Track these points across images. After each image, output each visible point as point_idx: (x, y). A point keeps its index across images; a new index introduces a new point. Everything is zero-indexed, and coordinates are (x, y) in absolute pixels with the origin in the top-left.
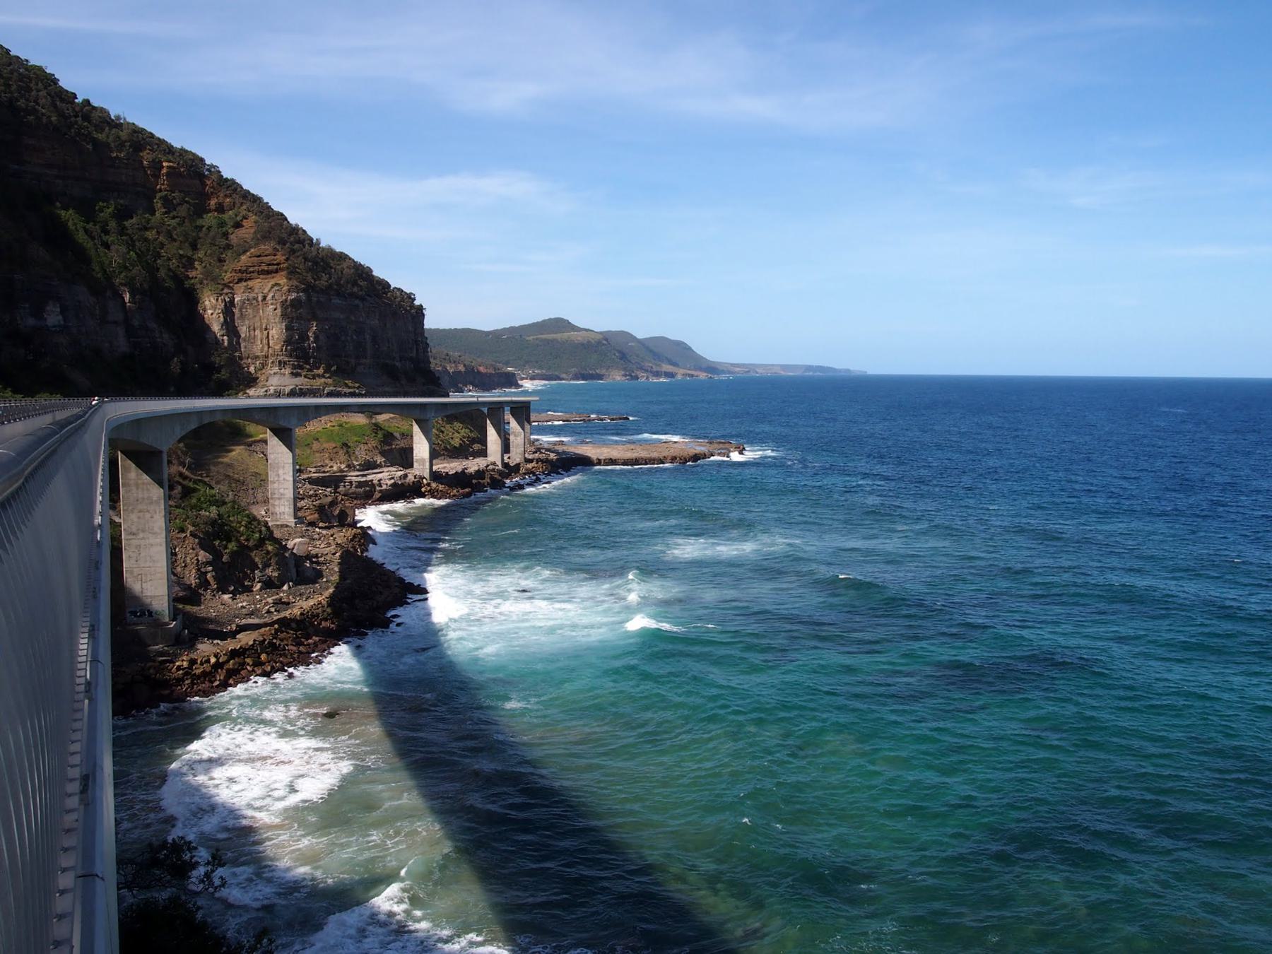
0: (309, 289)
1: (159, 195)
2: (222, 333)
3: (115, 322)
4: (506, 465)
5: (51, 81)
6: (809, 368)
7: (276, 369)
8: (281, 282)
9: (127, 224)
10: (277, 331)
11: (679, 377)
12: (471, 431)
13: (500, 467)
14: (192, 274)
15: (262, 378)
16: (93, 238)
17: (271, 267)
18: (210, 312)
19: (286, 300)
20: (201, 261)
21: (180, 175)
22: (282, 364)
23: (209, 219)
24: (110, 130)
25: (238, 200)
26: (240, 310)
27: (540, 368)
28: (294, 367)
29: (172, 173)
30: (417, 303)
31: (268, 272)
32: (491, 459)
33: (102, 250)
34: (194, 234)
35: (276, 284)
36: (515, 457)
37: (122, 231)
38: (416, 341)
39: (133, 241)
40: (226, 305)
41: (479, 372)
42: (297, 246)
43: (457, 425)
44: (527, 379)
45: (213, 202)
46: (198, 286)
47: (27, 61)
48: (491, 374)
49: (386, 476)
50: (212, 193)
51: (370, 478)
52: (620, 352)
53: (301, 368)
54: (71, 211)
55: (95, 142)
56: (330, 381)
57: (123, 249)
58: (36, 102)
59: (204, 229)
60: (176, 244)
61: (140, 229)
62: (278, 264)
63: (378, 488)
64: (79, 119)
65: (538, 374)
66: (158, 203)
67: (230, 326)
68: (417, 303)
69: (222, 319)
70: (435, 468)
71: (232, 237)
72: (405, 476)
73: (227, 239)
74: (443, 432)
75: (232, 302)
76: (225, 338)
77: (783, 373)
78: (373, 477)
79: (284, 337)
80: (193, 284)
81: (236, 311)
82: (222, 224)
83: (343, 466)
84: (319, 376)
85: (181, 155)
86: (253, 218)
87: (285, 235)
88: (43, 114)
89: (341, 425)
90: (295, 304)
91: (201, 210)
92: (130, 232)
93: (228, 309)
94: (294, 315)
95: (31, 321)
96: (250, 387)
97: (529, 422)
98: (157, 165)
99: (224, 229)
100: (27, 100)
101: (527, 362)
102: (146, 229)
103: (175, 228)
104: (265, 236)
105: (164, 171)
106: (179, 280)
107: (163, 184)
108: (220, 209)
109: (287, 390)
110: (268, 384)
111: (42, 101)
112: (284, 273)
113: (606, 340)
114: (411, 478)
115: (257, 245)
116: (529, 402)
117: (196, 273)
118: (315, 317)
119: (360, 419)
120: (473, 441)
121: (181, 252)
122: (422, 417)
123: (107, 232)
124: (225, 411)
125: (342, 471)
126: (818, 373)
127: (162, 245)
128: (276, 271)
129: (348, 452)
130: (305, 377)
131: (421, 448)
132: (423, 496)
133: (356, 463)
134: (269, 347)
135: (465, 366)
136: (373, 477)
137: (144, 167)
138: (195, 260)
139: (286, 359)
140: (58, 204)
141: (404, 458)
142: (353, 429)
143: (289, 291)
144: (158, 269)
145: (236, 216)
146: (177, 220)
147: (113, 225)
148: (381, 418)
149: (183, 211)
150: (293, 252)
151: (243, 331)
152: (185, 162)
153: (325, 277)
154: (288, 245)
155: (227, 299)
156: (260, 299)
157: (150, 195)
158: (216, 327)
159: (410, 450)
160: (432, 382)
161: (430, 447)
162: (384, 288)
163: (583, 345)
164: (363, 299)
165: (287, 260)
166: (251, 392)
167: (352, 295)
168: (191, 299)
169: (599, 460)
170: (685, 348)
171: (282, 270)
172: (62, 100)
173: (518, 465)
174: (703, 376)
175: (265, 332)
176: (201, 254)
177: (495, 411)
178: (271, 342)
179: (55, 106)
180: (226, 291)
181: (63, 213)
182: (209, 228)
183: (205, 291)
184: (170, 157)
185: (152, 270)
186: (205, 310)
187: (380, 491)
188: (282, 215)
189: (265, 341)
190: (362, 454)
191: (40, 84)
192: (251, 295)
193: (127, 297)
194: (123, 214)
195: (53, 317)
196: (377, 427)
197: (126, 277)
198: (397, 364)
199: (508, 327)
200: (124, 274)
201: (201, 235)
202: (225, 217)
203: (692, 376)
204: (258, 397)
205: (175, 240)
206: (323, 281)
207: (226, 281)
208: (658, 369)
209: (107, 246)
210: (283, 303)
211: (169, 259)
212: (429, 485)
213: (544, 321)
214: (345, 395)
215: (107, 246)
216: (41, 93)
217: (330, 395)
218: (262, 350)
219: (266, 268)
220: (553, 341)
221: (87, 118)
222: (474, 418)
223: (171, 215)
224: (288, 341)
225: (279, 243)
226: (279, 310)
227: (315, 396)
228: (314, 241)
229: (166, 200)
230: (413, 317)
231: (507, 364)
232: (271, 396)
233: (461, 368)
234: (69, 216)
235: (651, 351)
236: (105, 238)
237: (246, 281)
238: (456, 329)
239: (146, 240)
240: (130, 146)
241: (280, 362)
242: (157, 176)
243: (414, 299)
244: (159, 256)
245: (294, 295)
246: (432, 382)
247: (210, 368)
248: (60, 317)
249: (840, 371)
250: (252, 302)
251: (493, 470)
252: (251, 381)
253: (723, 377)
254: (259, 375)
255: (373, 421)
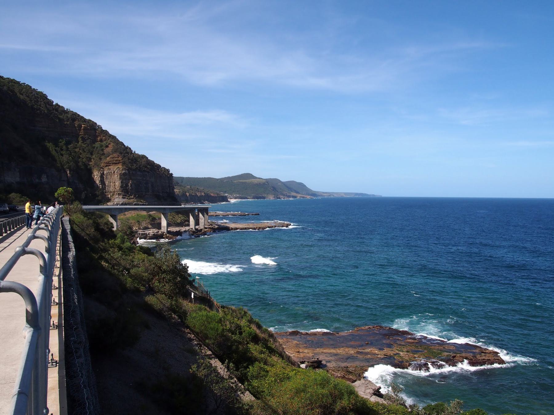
0: (129, 169)
1: (80, 136)
2: (100, 183)
3: (64, 181)
4: (196, 229)
5: (44, 97)
6: (357, 194)
7: (117, 196)
8: (120, 167)
9: (69, 146)
10: (118, 184)
11: (298, 198)
12: (185, 217)
13: (194, 230)
14: (91, 163)
15: (113, 199)
16: (57, 152)
17: (117, 162)
18: (96, 177)
19: (121, 173)
20: (94, 159)
21: (88, 129)
22: (119, 194)
23: (97, 145)
24: (65, 114)
25: (107, 137)
26: (106, 176)
27: (239, 194)
28: (123, 195)
29: (85, 129)
30: (170, 172)
31: (116, 163)
32: (191, 227)
33: (60, 156)
34: (92, 150)
35: (118, 168)
36: (201, 226)
37: (67, 149)
38: (169, 186)
39: (71, 153)
40: (101, 174)
41: (211, 196)
42: (126, 154)
43: (180, 215)
44: (233, 198)
45: (99, 138)
46: (92, 168)
47: (37, 90)
48: (216, 197)
49: (152, 232)
50: (99, 135)
51: (146, 232)
52: (273, 187)
53: (126, 196)
54: (51, 143)
55: (59, 119)
56: (135, 200)
57: (67, 156)
58: (40, 106)
59: (95, 148)
60: (86, 153)
61: (74, 148)
62: (119, 161)
63: (148, 236)
64: (54, 111)
65: (238, 197)
66: (80, 139)
67: (102, 181)
68: (170, 172)
69: (100, 179)
70: (168, 230)
71: (105, 151)
72: (158, 232)
73: (103, 151)
74: (174, 218)
75: (103, 174)
76: (101, 185)
77: (345, 196)
78: (147, 232)
79: (120, 185)
80: (91, 167)
81: (105, 176)
82: (102, 146)
83: (137, 228)
84: (132, 198)
85: (88, 122)
86: (112, 144)
87: (122, 151)
88: (42, 110)
89: (138, 215)
90: (124, 174)
91: (95, 141)
92: (70, 149)
93: (102, 176)
94: (124, 178)
95: (37, 180)
96: (108, 202)
97: (207, 214)
98: (80, 126)
99: (102, 148)
100: (37, 105)
101: (233, 192)
102: (76, 148)
103: (85, 148)
104: (115, 151)
105: (82, 128)
106: (86, 165)
107: (82, 132)
108: (101, 141)
109: (121, 203)
110: (114, 201)
111: (42, 106)
112: (121, 164)
113: (267, 182)
114: (160, 232)
115: (112, 154)
116: (208, 208)
117: (92, 163)
118: (131, 179)
119: (144, 213)
120: (186, 221)
121: (87, 156)
122: (164, 212)
123: (62, 150)
124: (94, 209)
125: (136, 230)
126: (360, 196)
127: (81, 154)
128: (119, 163)
129: (139, 224)
130: (127, 199)
131: (164, 223)
132: (163, 238)
133: (141, 227)
134: (115, 189)
135: (204, 193)
136: (147, 232)
137: (75, 127)
138: (92, 159)
139: (121, 193)
140: (47, 141)
141: (159, 226)
142: (142, 216)
143: (122, 170)
144: (79, 162)
145: (107, 143)
146: (86, 145)
147: (64, 147)
148: (151, 213)
149: (88, 141)
150: (124, 156)
151: (107, 183)
152: (90, 125)
153: (135, 165)
154: (123, 154)
155: (102, 173)
156: (113, 172)
157: (77, 136)
158: (98, 182)
159: (160, 224)
160: (173, 199)
161: (167, 222)
162: (158, 167)
163: (257, 184)
164: (148, 172)
165: (122, 159)
166: (109, 204)
167: (144, 171)
168: (90, 172)
169: (232, 228)
170: (303, 186)
171: (121, 163)
172: (49, 105)
173: (201, 230)
174: (308, 197)
175: (114, 184)
176: (94, 157)
177: (192, 210)
178: (116, 187)
179: (46, 107)
180: (101, 170)
181: (48, 144)
182: (97, 148)
183: (95, 169)
184: (84, 123)
185: (77, 162)
186: (94, 176)
187: (149, 237)
188: (122, 143)
189: (114, 187)
190: (144, 224)
191: (42, 100)
192: (110, 171)
193: (68, 172)
194: (68, 143)
195: (44, 179)
196: (150, 216)
197: (68, 166)
198: (161, 194)
199: (227, 177)
200: (67, 165)
201: (94, 150)
202: (103, 143)
203: (304, 197)
204: (111, 205)
205: (85, 152)
206: (134, 167)
207: (102, 166)
208: (289, 194)
209: (62, 155)
210: (120, 174)
211: (83, 158)
212: (166, 235)
213: (242, 174)
214: (140, 205)
215: (62, 155)
216: (42, 103)
217: (135, 205)
218: (113, 190)
219: (115, 162)
220: (245, 183)
221: (57, 110)
222: (186, 212)
223: (84, 143)
224: (121, 187)
225: (120, 153)
226: (119, 176)
227: (130, 205)
228: (133, 152)
229: (82, 138)
230: (168, 177)
231: (225, 192)
232: (115, 205)
233: (203, 194)
234: (50, 145)
235: (287, 187)
236: (62, 152)
237: (108, 166)
238: (205, 178)
239: (75, 152)
240: (71, 120)
241: (119, 194)
242: (80, 130)
243: (169, 171)
244: (80, 157)
245: (124, 171)
246: (173, 199)
247: (95, 196)
248: (47, 179)
249: (370, 195)
250: (110, 174)
251: (191, 231)
252: (109, 200)
253: (320, 198)
254: (111, 198)
255: (149, 214)
